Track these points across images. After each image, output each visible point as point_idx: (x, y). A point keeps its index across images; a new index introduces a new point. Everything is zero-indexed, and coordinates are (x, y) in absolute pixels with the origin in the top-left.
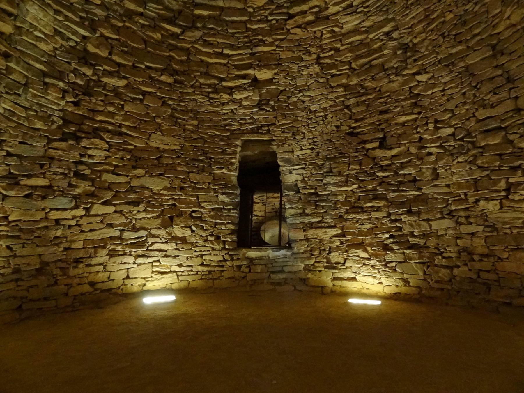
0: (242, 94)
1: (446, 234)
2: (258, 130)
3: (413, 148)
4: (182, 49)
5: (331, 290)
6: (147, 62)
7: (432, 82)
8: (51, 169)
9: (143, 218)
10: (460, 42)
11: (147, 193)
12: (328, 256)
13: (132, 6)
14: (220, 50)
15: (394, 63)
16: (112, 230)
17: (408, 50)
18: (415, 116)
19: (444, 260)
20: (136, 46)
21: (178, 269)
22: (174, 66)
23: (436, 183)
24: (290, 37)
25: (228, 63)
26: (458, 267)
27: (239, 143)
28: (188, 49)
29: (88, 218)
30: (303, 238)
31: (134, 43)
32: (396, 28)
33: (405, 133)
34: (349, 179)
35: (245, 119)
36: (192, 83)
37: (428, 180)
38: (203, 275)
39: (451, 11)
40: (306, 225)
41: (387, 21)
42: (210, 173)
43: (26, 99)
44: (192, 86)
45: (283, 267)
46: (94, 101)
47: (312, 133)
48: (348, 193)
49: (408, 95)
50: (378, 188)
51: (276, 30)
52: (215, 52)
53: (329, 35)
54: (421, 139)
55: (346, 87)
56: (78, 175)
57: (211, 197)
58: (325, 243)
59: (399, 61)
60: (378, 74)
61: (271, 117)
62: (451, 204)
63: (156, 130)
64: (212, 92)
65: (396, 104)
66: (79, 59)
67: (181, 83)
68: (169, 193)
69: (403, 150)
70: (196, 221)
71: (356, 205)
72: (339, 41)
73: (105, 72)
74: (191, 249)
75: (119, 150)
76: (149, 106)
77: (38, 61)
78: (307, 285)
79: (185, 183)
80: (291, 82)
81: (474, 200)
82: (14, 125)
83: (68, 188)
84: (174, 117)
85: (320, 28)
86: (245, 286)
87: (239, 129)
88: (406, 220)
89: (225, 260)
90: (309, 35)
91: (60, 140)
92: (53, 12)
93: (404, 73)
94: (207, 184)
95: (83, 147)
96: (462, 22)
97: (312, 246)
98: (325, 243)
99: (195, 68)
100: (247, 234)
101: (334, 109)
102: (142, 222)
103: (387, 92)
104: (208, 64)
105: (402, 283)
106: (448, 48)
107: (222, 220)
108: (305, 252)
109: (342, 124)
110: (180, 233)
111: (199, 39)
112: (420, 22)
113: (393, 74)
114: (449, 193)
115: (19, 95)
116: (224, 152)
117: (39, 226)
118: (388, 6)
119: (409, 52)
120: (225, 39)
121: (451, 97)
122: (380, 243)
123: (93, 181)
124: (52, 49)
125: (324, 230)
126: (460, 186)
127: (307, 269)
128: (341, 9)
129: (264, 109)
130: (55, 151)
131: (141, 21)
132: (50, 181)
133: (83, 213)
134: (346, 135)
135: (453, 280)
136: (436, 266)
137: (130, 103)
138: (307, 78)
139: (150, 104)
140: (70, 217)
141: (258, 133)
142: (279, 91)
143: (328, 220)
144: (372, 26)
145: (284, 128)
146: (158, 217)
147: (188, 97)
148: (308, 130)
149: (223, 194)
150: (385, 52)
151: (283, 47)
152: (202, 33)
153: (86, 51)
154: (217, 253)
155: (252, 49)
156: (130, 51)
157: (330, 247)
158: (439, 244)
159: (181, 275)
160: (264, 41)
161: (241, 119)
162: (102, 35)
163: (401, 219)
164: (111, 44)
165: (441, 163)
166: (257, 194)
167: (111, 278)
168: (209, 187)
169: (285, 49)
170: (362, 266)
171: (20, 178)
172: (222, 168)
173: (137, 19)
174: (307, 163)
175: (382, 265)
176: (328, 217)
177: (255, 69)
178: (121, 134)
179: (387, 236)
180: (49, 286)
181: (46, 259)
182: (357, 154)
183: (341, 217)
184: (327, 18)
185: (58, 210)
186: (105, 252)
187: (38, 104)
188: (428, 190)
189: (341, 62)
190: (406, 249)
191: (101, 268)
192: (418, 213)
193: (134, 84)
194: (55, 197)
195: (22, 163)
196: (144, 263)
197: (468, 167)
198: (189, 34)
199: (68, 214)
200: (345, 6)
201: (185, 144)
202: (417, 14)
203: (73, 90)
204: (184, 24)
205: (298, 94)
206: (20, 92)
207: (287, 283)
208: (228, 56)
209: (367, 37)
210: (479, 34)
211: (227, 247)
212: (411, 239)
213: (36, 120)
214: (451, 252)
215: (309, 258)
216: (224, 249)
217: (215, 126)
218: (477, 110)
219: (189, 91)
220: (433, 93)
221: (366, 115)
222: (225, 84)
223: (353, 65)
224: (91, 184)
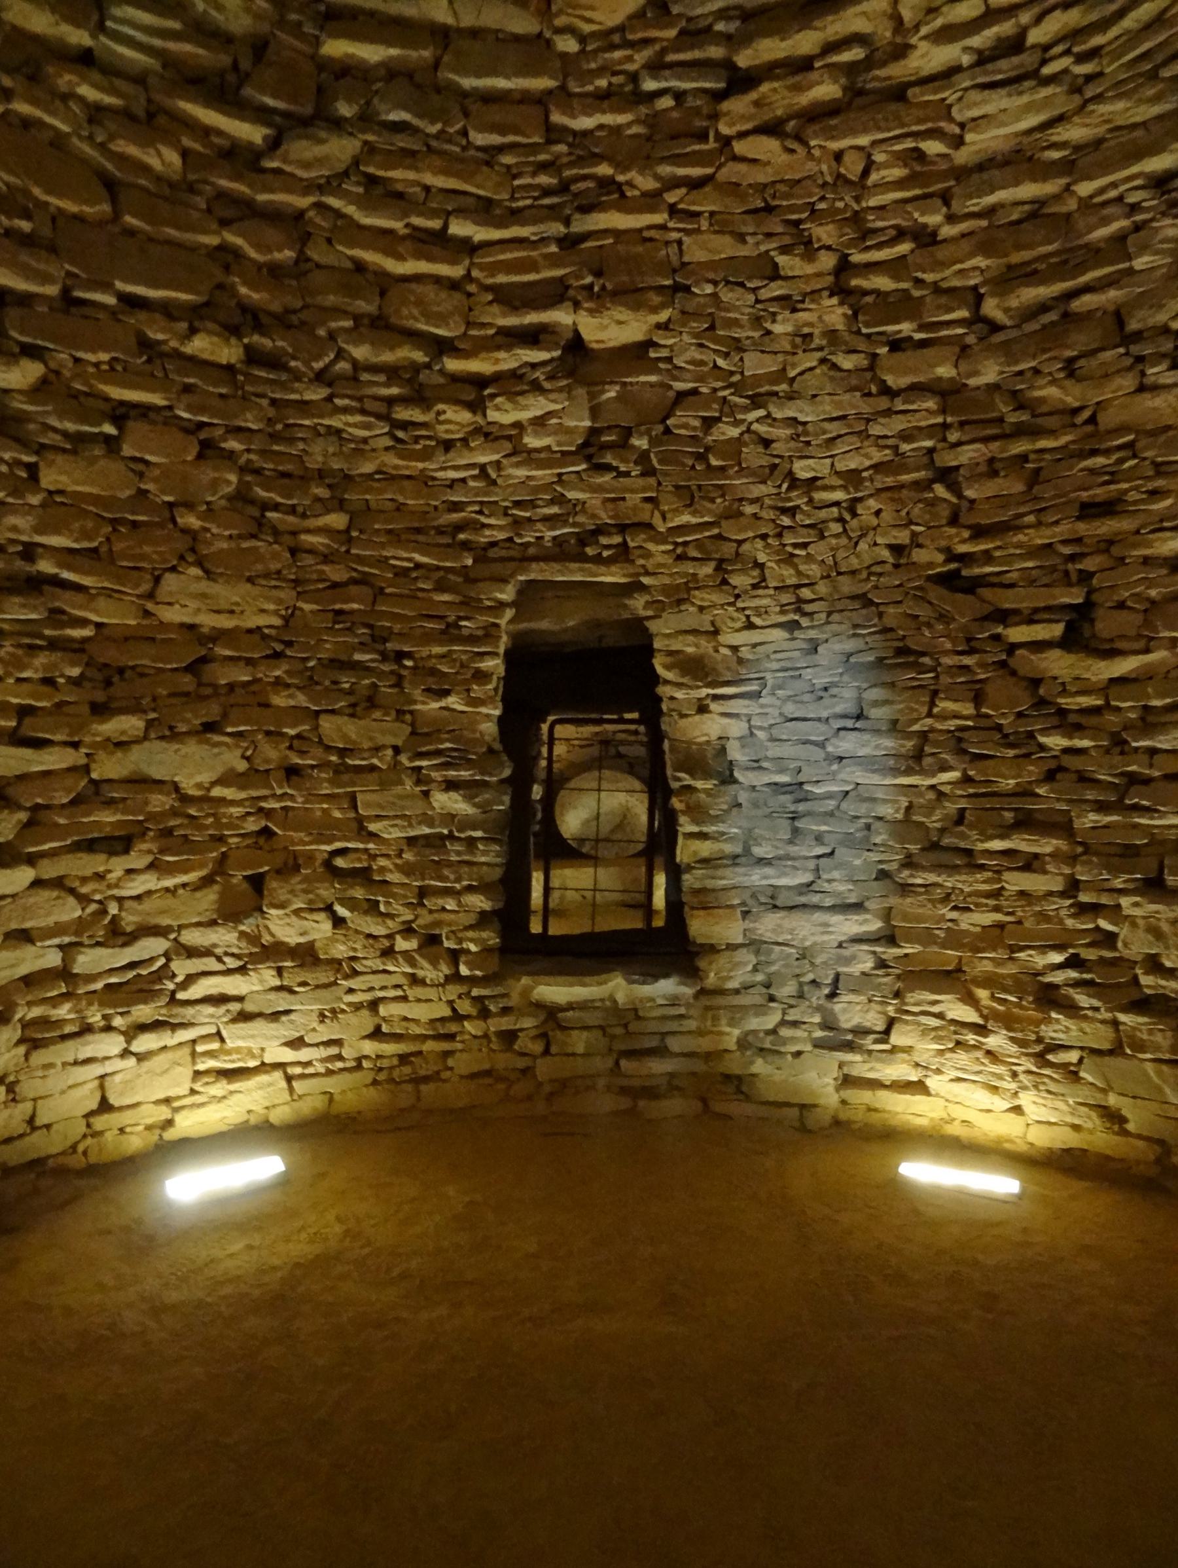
0: (525, 408)
4: (274, 216)
6: (125, 280)
9: (149, 893)
11: (160, 802)
12: (829, 1005)
13: (40, 22)
14: (435, 224)
16: (29, 950)
20: (71, 207)
21: (288, 1055)
22: (243, 290)
24: (729, 172)
25: (468, 277)
27: (507, 594)
28: (300, 215)
31: (60, 196)
35: (532, 504)
36: (318, 365)
38: (381, 1069)
42: (400, 713)
44: (320, 377)
45: (664, 1035)
47: (795, 567)
48: (921, 795)
50: (1041, 791)
51: (673, 138)
52: (416, 228)
53: (897, 173)
55: (948, 394)
58: (818, 961)
60: (1094, 352)
61: (634, 499)
63: (182, 558)
67: (274, 362)
68: (243, 795)
69: (1162, 662)
70: (352, 887)
71: (946, 841)
74: (335, 983)
79: (302, 753)
80: (721, 362)
85: (864, 141)
86: (529, 1098)
87: (510, 540)
88: (1137, 912)
89: (457, 1017)
90: (811, 167)
94: (390, 752)
97: (773, 968)
99: (331, 300)
104: (385, 283)
105: (1098, 1122)
107: (441, 878)
109: (916, 542)
111: (346, 174)
113: (1164, 356)
116: (450, 633)
120: (458, 175)
125: (819, 917)
128: (966, 60)
129: (608, 468)
131: (86, 91)
134: (929, 585)
137: (60, 459)
138: (788, 348)
139: (148, 457)
141: (583, 558)
142: (671, 394)
144: (1098, 142)
145: (685, 543)
146: (206, 882)
147: (307, 422)
148: (777, 553)
149: (451, 785)
150: (1141, 263)
151: (698, 214)
152: (357, 144)
154: (431, 993)
155: (567, 222)
156: (46, 232)
159: (303, 1076)
161: (518, 504)
167: (39, 1122)
168: (396, 764)
169: (705, 224)
172: (446, 693)
173: (66, 80)
175: (1027, 1055)
176: (836, 874)
177: (577, 305)
178: (36, 584)
179: (1057, 958)
182: (967, 661)
184: (898, 93)
189: (937, 289)
190: (1125, 1010)
193: (76, 376)
198: (301, 149)
200: (989, 44)
201: (300, 604)
204: (280, 105)
205: (746, 409)
207: (678, 1088)
208: (469, 248)
209: (1067, 188)
212: (1146, 980)
216: (455, 978)
219: (310, 396)
222: (453, 365)
223: (991, 308)
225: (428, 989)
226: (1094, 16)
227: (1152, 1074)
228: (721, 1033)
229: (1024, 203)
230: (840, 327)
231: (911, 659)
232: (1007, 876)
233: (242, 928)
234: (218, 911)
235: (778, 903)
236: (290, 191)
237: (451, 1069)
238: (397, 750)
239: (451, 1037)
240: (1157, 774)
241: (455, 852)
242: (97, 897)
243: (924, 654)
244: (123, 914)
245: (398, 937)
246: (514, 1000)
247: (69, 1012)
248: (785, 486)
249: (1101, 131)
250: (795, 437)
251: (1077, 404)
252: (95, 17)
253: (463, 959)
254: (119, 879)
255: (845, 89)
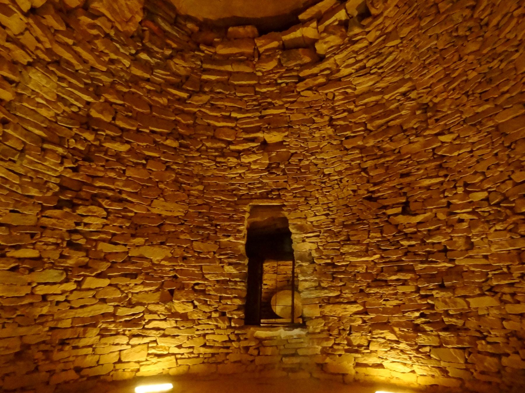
0: (251, 158)
1: (488, 314)
2: (268, 194)
3: (441, 214)
4: (189, 113)
5: (354, 378)
7: (457, 142)
8: (42, 239)
9: (141, 292)
10: (487, 100)
12: (349, 337)
14: (228, 114)
15: (414, 124)
16: (105, 306)
17: (428, 109)
18: (441, 179)
19: (489, 346)
21: (177, 351)
22: (180, 130)
23: (471, 253)
25: (236, 126)
26: (507, 355)
27: (247, 208)
28: (195, 113)
29: (78, 293)
30: (319, 315)
31: (139, 108)
32: (413, 88)
33: (430, 197)
34: (370, 249)
35: (254, 184)
36: (197, 147)
37: (462, 250)
38: (205, 358)
39: (474, 69)
40: (323, 300)
41: (404, 81)
42: (216, 242)
43: (21, 165)
44: (198, 150)
46: (95, 166)
47: (327, 198)
48: (369, 263)
49: (431, 157)
50: (403, 259)
53: (342, 97)
54: (449, 204)
55: (362, 149)
56: (71, 245)
57: (216, 267)
58: (344, 321)
59: (418, 122)
62: (491, 279)
63: (159, 196)
64: (219, 156)
65: (419, 166)
66: (81, 124)
67: (187, 147)
68: (170, 264)
69: (430, 216)
71: (379, 278)
72: (352, 103)
73: (107, 137)
74: (192, 327)
75: (118, 217)
76: (153, 171)
77: (37, 127)
78: (325, 372)
79: (188, 252)
80: (302, 145)
81: (520, 275)
82: (6, 192)
83: (59, 260)
84: (178, 182)
85: (332, 90)
86: (253, 371)
87: (248, 194)
89: (230, 341)
90: (320, 97)
91: (55, 208)
92: (57, 78)
93: (425, 134)
94: (212, 253)
95: (79, 214)
96: (488, 80)
97: (330, 325)
98: (344, 321)
99: (202, 132)
100: (256, 309)
101: (349, 172)
102: (139, 296)
103: (407, 153)
104: (215, 128)
105: (439, 373)
106: (473, 106)
108: (322, 331)
110: (181, 309)
111: (206, 104)
112: (440, 81)
113: (414, 134)
114: (488, 265)
115: (14, 162)
116: (231, 219)
117: (23, 303)
118: (403, 66)
119: (429, 112)
120: (233, 102)
121: (482, 158)
122: (409, 322)
123: (87, 251)
124: (54, 115)
126: (500, 257)
127: (325, 352)
128: (353, 71)
129: (274, 173)
130: (49, 219)
132: (40, 252)
133: (74, 287)
135: (503, 372)
136: (479, 352)
137: (131, 168)
139: (154, 169)
140: (60, 292)
142: (290, 154)
143: (348, 294)
144: (387, 87)
145: (296, 193)
146: (157, 290)
149: (230, 264)
150: (403, 112)
151: (293, 109)
153: (89, 116)
155: (261, 112)
157: (351, 327)
158: (480, 326)
159: (181, 358)
160: (273, 104)
161: (250, 184)
162: (106, 101)
163: (432, 295)
164: (115, 109)
165: (475, 231)
166: (267, 262)
167: (100, 363)
168: (215, 257)
169: (295, 111)
170: (389, 351)
171: (7, 250)
172: (229, 236)
173: (143, 84)
174: (322, 230)
176: (347, 291)
177: (264, 132)
178: (121, 201)
179: (417, 314)
180: (27, 373)
181: (27, 340)
183: (362, 291)
184: (339, 80)
185: (45, 284)
186: (96, 331)
187: (34, 170)
188: (461, 261)
189: (355, 123)
190: (441, 331)
191: (91, 349)
192: (453, 289)
193: (137, 149)
194: (44, 269)
195: (10, 234)
196: (139, 344)
197: (508, 235)
198: (196, 98)
199: (57, 289)
200: (358, 68)
201: (190, 210)
202: (436, 73)
203: (73, 155)
205: (310, 156)
206: (15, 159)
208: (236, 119)
209: (383, 98)
210: (507, 92)
211: (233, 325)
212: (446, 319)
213: (30, 187)
214: (496, 336)
215: (327, 339)
216: (230, 327)
217: (221, 191)
218: (513, 172)
220: (459, 154)
221: (385, 179)
222: (232, 147)
223: (369, 126)
224: (85, 254)
225: (222, 330)
226: (380, 60)
227: (453, 353)
228: (315, 348)
229: (373, 102)
230: (332, 134)
231: (361, 222)
232: (398, 287)
233: (166, 306)
234: (159, 300)
235: (330, 302)
236: (192, 107)
237: (228, 359)
238: (215, 253)
239: (228, 348)
240: (436, 250)
241: (231, 285)
242: (126, 292)
243: (365, 220)
244: (133, 298)
245: (213, 313)
246: (248, 336)
247: (114, 327)
248: (322, 176)
249: (387, 84)
250: (324, 163)
251: (394, 148)
252: (151, 72)
253: (232, 320)
254: (133, 287)
255: (326, 79)
